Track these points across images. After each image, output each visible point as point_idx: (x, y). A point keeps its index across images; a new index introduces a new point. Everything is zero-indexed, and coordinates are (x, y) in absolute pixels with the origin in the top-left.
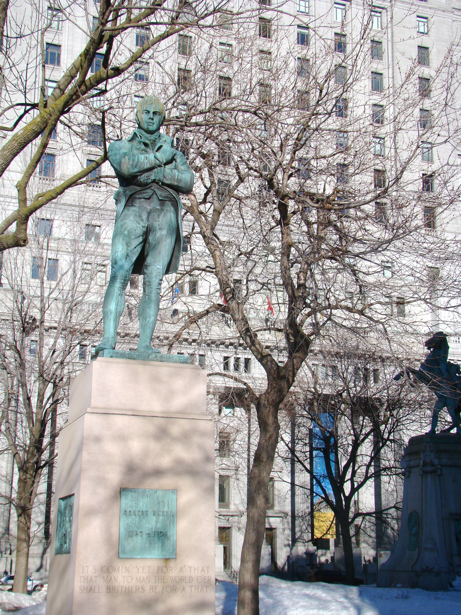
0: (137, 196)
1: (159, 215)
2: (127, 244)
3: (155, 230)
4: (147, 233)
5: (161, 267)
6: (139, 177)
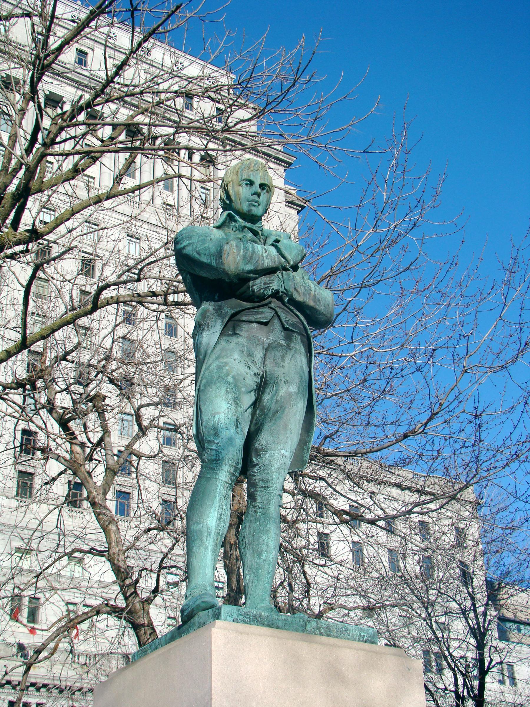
0: (244, 318)
1: (283, 356)
2: (235, 401)
3: (276, 383)
4: (262, 385)
5: (288, 454)
6: (251, 283)
